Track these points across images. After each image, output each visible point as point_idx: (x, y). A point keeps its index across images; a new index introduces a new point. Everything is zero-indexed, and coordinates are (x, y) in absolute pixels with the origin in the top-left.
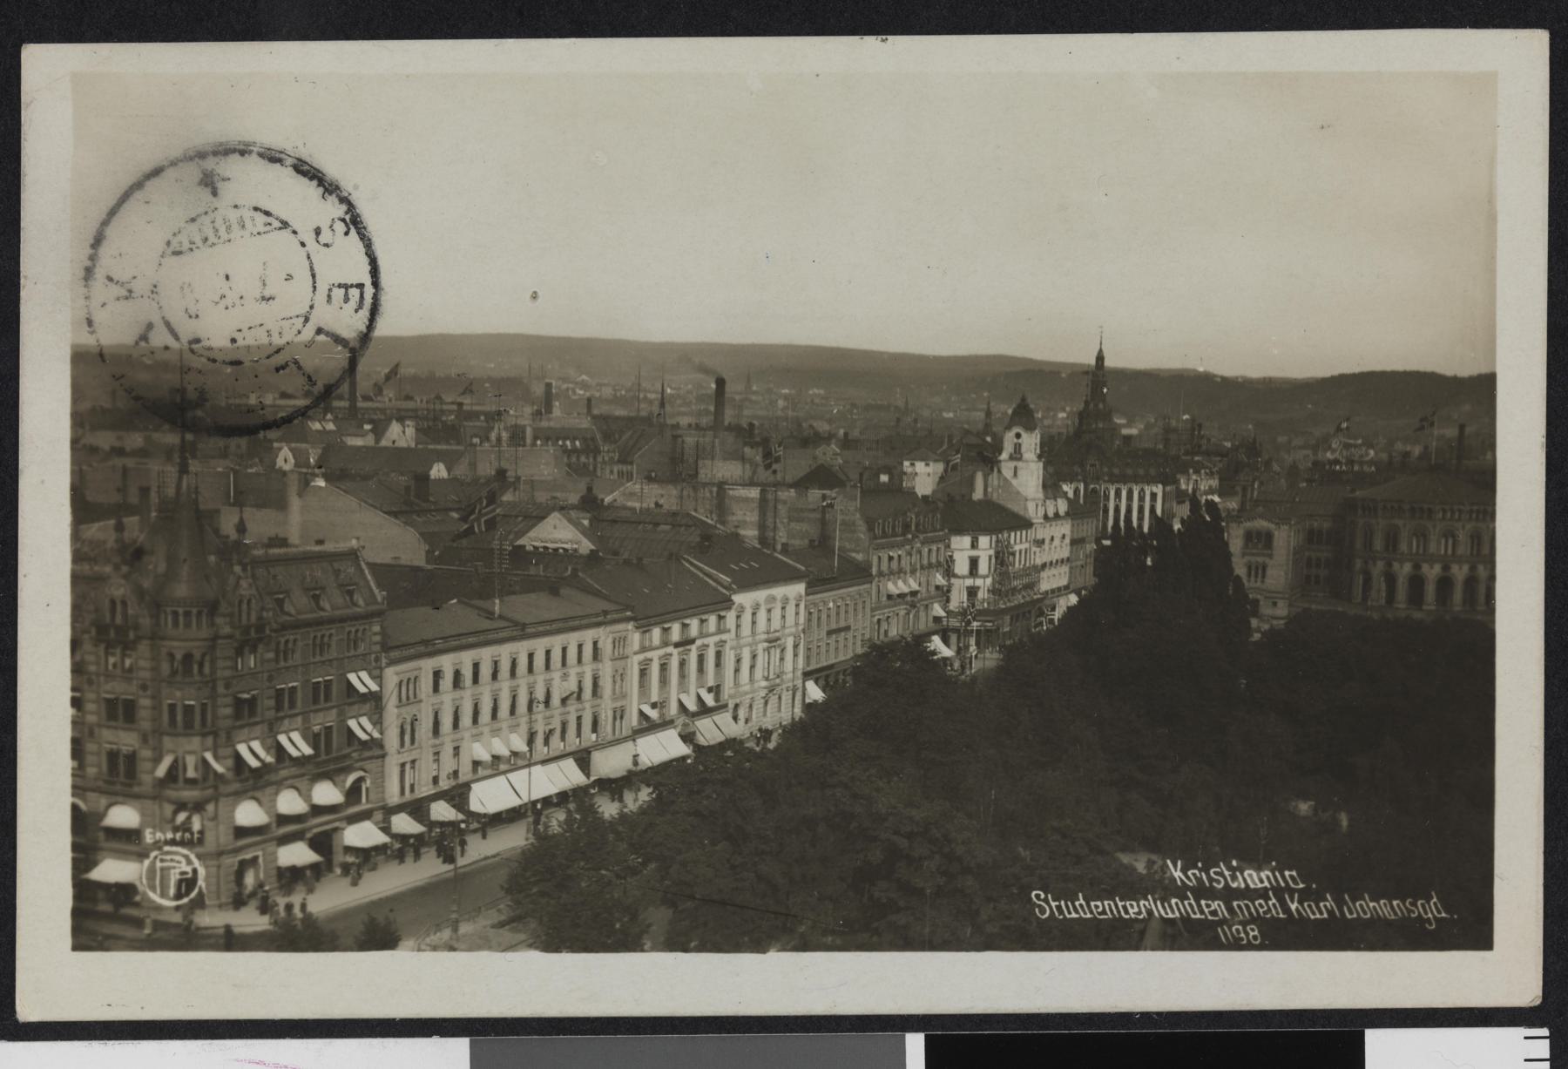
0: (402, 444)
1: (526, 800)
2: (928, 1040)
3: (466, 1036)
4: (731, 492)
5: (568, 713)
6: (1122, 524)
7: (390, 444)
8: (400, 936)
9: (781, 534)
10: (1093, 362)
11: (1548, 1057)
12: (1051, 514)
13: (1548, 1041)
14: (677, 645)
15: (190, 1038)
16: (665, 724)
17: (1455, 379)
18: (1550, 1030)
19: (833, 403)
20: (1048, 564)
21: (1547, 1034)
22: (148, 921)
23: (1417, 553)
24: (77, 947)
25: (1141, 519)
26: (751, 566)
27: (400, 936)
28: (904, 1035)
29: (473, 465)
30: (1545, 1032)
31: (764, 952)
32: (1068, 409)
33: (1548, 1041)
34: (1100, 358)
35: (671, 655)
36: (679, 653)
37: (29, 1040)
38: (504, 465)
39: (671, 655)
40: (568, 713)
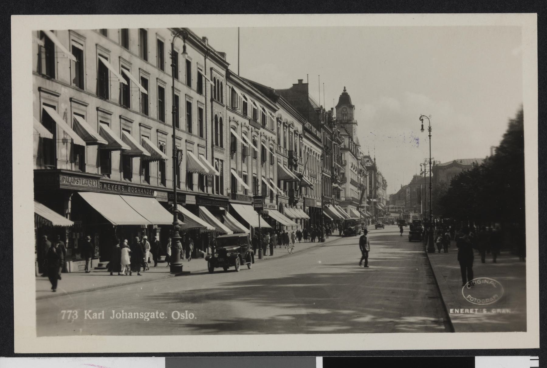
3: (164, 356)
8: (460, 174)
11: (538, 366)
13: (538, 361)
19: (313, 230)
21: (538, 359)
27: (460, 174)
28: (315, 358)
30: (537, 358)
31: (349, 96)
33: (538, 361)
34: (416, 174)
37: (13, 357)
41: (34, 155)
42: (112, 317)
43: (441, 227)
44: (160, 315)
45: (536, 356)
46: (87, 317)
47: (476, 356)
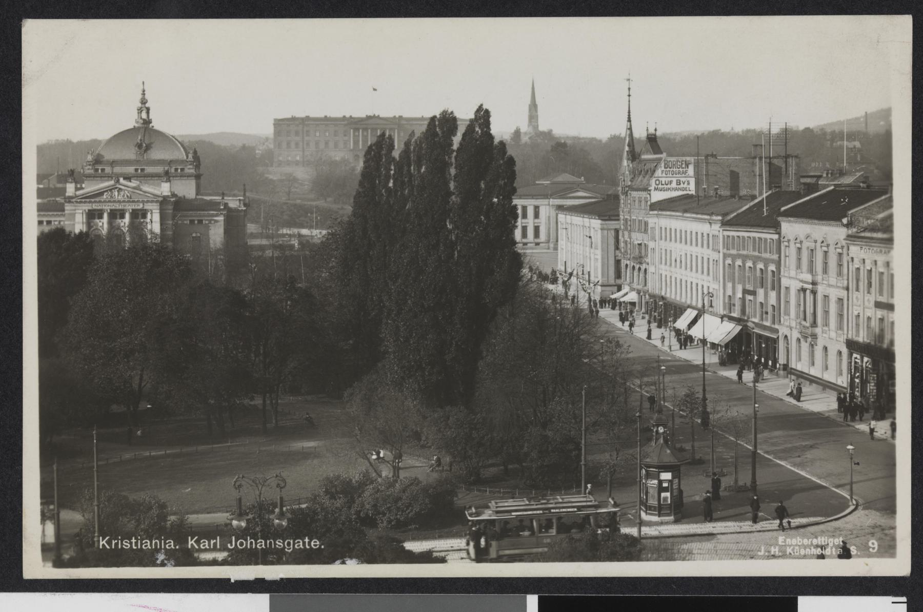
2: (540, 599)
3: (267, 593)
15: (104, 592)
18: (907, 598)
22: (552, 249)
24: (275, 120)
28: (526, 597)
30: (904, 599)
37: (9, 592)
41: (892, 244)
42: (232, 545)
43: (623, 470)
44: (312, 543)
45: (902, 596)
46: (103, 545)
47: (800, 595)
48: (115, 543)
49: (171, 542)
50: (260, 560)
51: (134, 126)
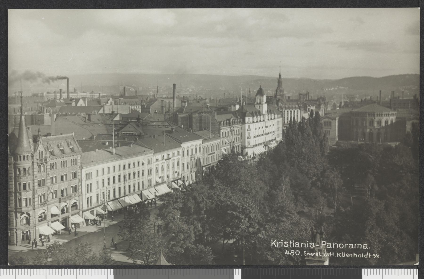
0: (83, 105)
1: (124, 206)
4: (179, 116)
5: (135, 180)
6: (292, 120)
7: (80, 106)
9: (194, 127)
10: (278, 76)
12: (270, 119)
14: (166, 160)
16: (163, 183)
17: (376, 78)
20: (269, 133)
23: (237, 134)
25: (297, 119)
26: (185, 136)
29: (104, 110)
30: (363, 269)
32: (271, 90)
35: (164, 162)
36: (167, 162)
38: (114, 110)
39: (164, 162)
40: (135, 180)
48: (279, 244)
49: (366, 245)
50: (120, 145)
51: (140, 201)
